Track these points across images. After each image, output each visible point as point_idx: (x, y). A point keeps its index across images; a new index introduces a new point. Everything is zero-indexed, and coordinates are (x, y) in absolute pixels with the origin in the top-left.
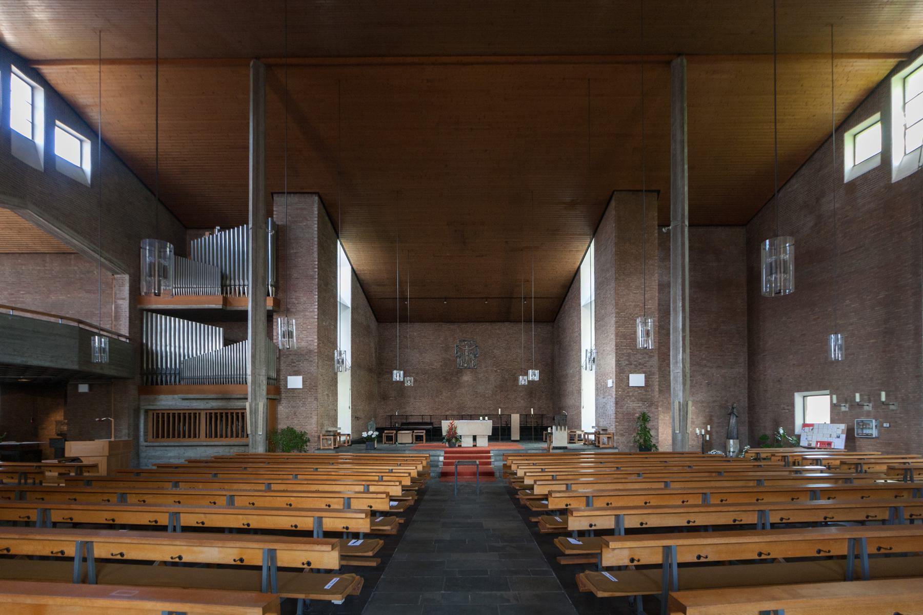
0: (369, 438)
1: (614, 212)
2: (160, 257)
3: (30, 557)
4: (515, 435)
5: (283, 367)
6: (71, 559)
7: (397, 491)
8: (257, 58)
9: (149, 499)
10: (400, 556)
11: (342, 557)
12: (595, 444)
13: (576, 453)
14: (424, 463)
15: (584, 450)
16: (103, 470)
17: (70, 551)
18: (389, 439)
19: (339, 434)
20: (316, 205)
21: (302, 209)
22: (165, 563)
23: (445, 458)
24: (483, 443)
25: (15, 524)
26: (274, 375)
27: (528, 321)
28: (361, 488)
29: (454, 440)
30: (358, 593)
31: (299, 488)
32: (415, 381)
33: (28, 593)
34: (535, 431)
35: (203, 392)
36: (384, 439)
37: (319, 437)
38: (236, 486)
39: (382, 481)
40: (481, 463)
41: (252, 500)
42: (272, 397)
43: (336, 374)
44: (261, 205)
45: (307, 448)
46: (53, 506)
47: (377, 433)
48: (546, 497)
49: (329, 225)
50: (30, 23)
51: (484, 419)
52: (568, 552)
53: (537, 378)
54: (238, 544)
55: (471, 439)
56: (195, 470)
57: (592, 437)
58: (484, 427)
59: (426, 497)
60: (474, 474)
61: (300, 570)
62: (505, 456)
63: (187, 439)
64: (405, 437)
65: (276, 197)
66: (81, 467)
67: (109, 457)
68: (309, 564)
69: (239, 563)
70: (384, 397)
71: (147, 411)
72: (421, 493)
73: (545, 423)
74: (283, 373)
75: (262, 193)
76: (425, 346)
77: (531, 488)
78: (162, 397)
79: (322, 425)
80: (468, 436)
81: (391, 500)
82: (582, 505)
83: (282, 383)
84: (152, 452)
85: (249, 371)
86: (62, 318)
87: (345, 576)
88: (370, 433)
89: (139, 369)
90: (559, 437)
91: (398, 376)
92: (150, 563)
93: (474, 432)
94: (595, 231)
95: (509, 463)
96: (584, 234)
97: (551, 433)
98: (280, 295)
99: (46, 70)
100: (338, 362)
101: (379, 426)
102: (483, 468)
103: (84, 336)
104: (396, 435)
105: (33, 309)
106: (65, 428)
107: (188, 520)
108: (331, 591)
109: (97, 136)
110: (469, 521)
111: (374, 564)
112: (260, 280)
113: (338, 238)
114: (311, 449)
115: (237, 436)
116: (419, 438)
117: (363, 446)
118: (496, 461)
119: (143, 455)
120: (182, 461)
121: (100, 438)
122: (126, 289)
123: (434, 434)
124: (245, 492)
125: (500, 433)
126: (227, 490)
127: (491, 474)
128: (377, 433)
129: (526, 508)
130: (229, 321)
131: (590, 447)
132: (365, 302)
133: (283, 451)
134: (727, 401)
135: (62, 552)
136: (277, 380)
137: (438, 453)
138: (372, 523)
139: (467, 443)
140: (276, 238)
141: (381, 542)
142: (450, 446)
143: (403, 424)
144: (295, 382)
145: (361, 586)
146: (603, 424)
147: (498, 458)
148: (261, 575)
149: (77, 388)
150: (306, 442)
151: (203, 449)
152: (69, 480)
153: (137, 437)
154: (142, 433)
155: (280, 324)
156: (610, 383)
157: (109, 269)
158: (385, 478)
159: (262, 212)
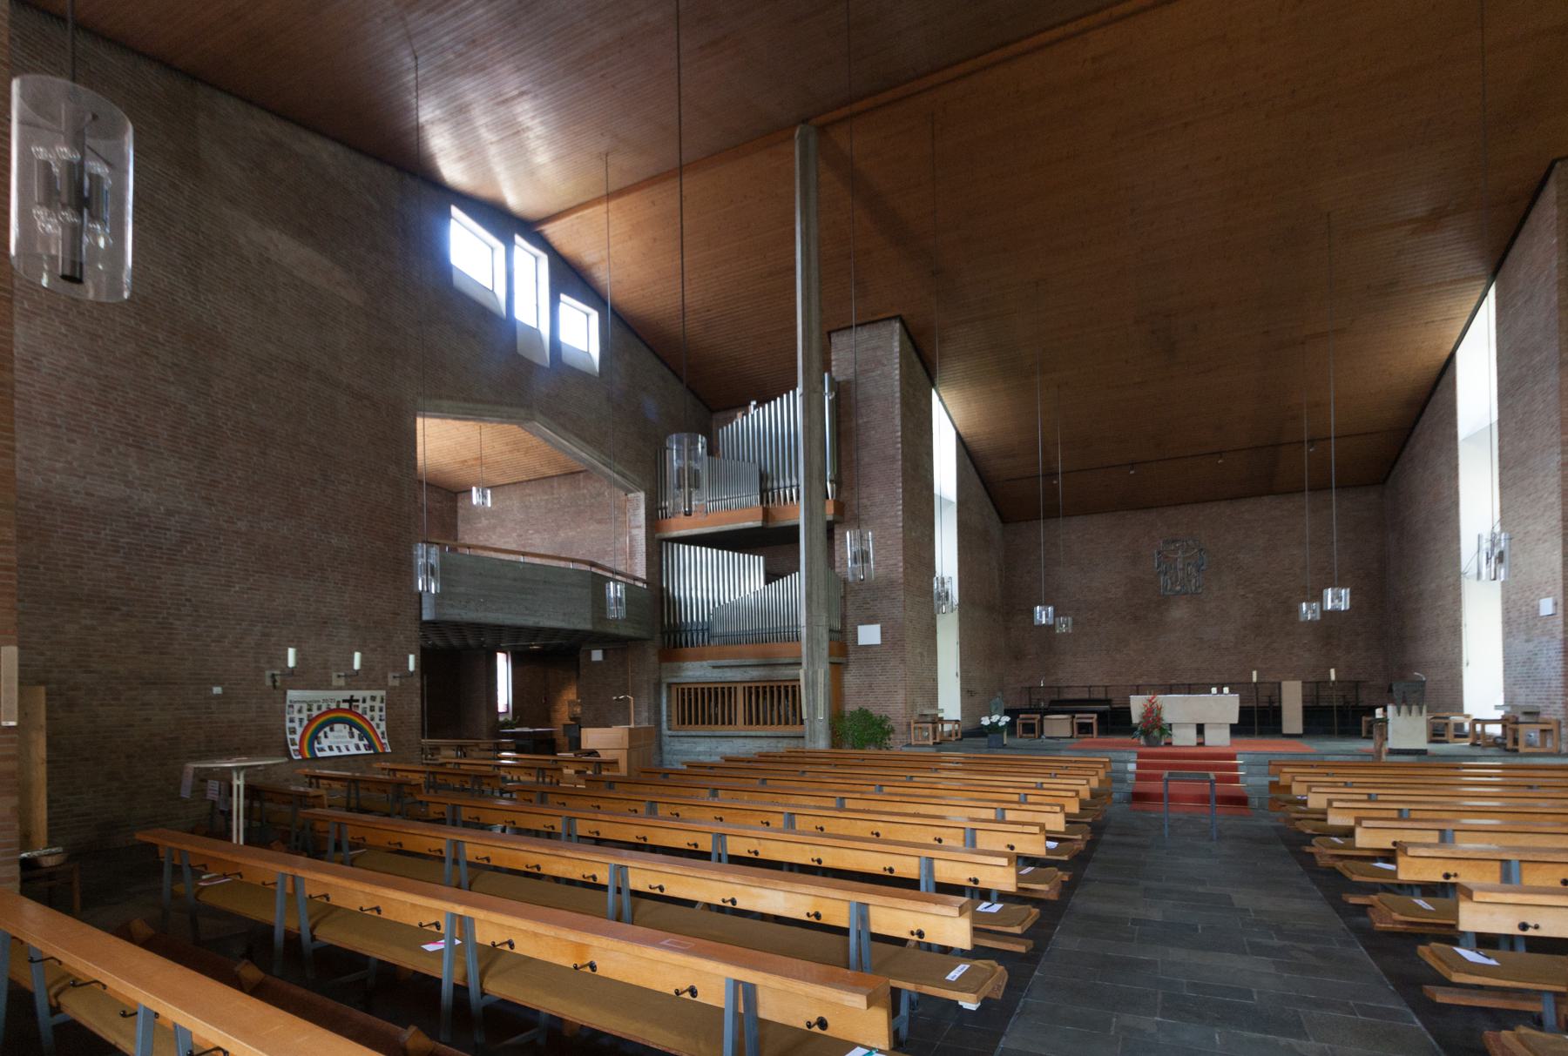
0: (994, 727)
1: (1555, 211)
2: (690, 458)
3: (557, 879)
4: (1293, 719)
5: (851, 611)
6: (604, 888)
7: (1057, 823)
8: (805, 121)
9: (684, 812)
10: (1064, 941)
11: (976, 931)
12: (1508, 744)
13: (1452, 764)
14: (1102, 773)
15: (1474, 758)
16: (623, 769)
17: (604, 877)
18: (1029, 729)
19: (941, 720)
20: (897, 338)
21: (875, 349)
22: (709, 906)
23: (1139, 766)
24: (1218, 738)
25: (537, 834)
26: (838, 626)
27: (1320, 487)
28: (991, 814)
29: (1156, 733)
30: (999, 995)
31: (888, 807)
32: (1075, 623)
33: (572, 927)
34: (1340, 715)
35: (739, 655)
36: (1019, 729)
37: (909, 725)
38: (794, 800)
39: (1026, 802)
40: (1220, 779)
41: (820, 822)
42: (835, 660)
43: (934, 618)
44: (816, 356)
45: (890, 743)
46: (580, 814)
47: (1007, 719)
48: (1389, 856)
49: (919, 366)
50: (532, 172)
51: (1220, 691)
52: (1457, 978)
53: (1344, 605)
54: (813, 890)
55: (1194, 732)
56: (735, 773)
57: (1496, 730)
58: (1222, 707)
59: (1106, 837)
60: (1204, 799)
61: (901, 942)
62: (1276, 766)
63: (719, 727)
64: (1058, 725)
65: (835, 338)
66: (600, 763)
67: (630, 749)
68: (921, 934)
69: (813, 919)
70: (1018, 655)
71: (669, 686)
72: (1097, 829)
73: (1365, 699)
74: (850, 621)
75: (815, 335)
76: (1091, 560)
77: (1349, 833)
78: (688, 665)
79: (914, 705)
80: (1185, 725)
81: (1049, 839)
82: (1492, 875)
83: (850, 636)
84: (678, 745)
85: (803, 621)
86: (573, 561)
87: (977, 963)
88: (995, 718)
89: (661, 625)
90: (1405, 729)
91: (1043, 615)
92: (691, 904)
93: (1202, 717)
94: (1496, 267)
95: (1284, 780)
96: (1474, 278)
97: (1385, 721)
98: (845, 494)
99: (550, 230)
100: (939, 597)
101: (1009, 706)
102: (1223, 789)
103: (597, 583)
104: (1041, 722)
105: (542, 552)
106: (578, 710)
107: (738, 847)
108: (957, 985)
109: (606, 303)
110: (1200, 889)
111: (1022, 949)
112: (816, 473)
113: (933, 385)
114: (897, 744)
115: (787, 723)
116: (1084, 729)
117: (983, 741)
118: (1249, 774)
119: (666, 748)
120: (716, 759)
121: (617, 724)
122: (642, 512)
123: (1115, 721)
124: (809, 808)
125: (1258, 718)
126: (786, 805)
127: (1240, 801)
128: (1007, 719)
129: (1334, 873)
130: (770, 543)
131: (1491, 751)
132: (982, 492)
133: (854, 747)
134: (170, 513)
135: (594, 877)
136: (842, 632)
137: (1125, 756)
138: (1020, 878)
139: (1184, 738)
140: (836, 404)
141: (1035, 911)
142: (1149, 745)
143: (1053, 702)
144: (869, 635)
145: (1003, 985)
146: (1525, 699)
147: (1254, 769)
148: (847, 944)
149: (589, 655)
150: (888, 733)
151: (740, 741)
152: (588, 780)
153: (659, 723)
154: (664, 718)
155: (849, 542)
156: (1546, 606)
157: (622, 487)
158: (1031, 799)
159: (816, 364)
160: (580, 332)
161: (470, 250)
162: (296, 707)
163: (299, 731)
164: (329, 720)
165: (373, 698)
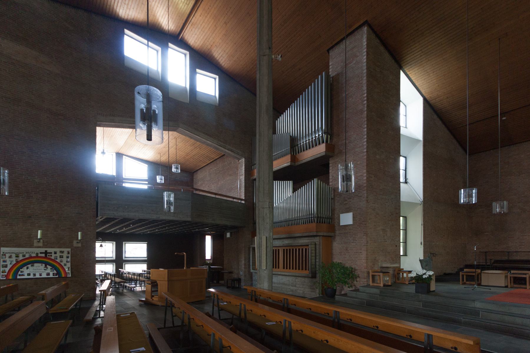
37: (368, 273)
49: (387, 55)
113: (401, 67)
119: (254, 278)
151: (280, 277)
160: (208, 85)
161: (136, 50)
162: (8, 255)
163: (9, 266)
164: (31, 261)
165: (62, 252)
